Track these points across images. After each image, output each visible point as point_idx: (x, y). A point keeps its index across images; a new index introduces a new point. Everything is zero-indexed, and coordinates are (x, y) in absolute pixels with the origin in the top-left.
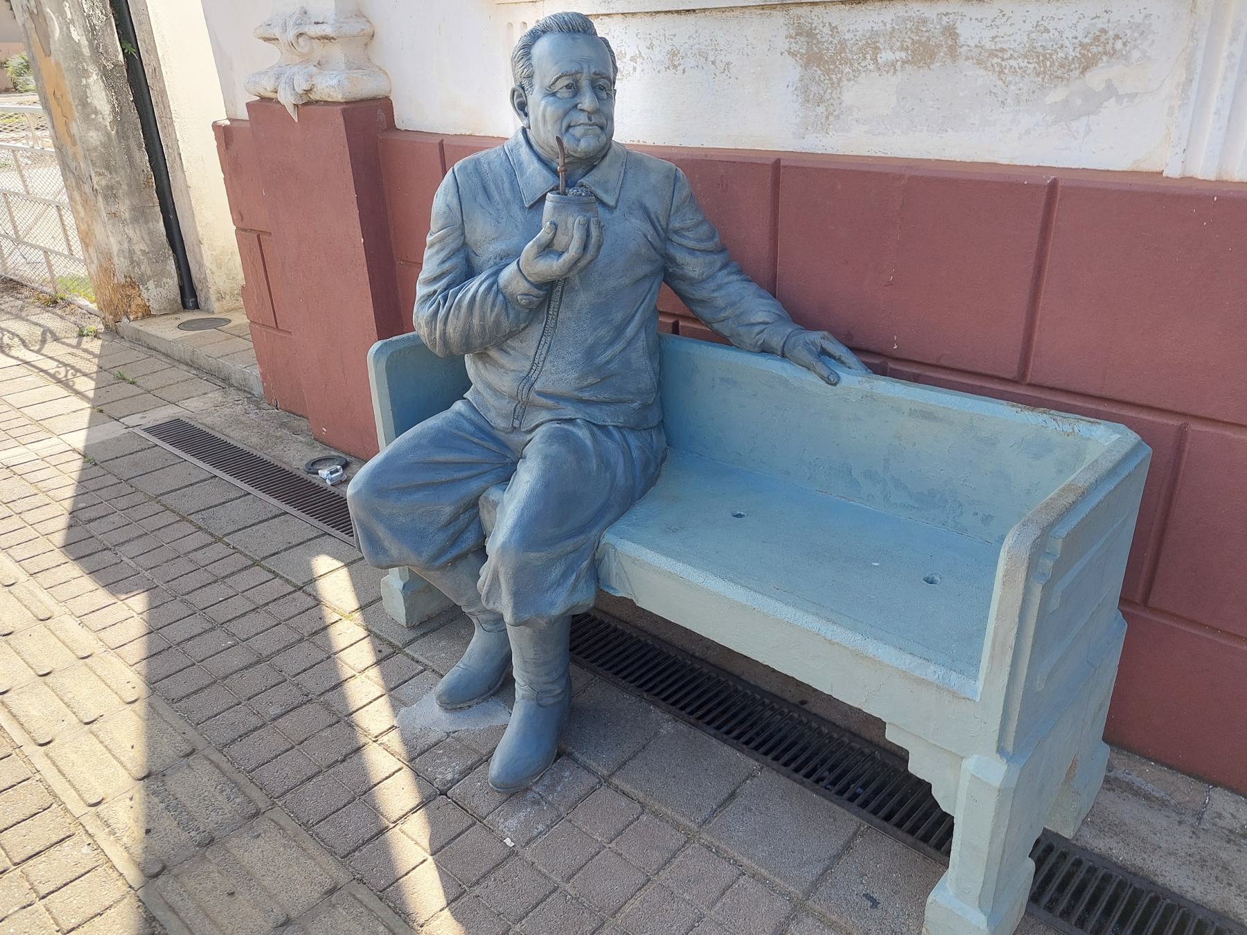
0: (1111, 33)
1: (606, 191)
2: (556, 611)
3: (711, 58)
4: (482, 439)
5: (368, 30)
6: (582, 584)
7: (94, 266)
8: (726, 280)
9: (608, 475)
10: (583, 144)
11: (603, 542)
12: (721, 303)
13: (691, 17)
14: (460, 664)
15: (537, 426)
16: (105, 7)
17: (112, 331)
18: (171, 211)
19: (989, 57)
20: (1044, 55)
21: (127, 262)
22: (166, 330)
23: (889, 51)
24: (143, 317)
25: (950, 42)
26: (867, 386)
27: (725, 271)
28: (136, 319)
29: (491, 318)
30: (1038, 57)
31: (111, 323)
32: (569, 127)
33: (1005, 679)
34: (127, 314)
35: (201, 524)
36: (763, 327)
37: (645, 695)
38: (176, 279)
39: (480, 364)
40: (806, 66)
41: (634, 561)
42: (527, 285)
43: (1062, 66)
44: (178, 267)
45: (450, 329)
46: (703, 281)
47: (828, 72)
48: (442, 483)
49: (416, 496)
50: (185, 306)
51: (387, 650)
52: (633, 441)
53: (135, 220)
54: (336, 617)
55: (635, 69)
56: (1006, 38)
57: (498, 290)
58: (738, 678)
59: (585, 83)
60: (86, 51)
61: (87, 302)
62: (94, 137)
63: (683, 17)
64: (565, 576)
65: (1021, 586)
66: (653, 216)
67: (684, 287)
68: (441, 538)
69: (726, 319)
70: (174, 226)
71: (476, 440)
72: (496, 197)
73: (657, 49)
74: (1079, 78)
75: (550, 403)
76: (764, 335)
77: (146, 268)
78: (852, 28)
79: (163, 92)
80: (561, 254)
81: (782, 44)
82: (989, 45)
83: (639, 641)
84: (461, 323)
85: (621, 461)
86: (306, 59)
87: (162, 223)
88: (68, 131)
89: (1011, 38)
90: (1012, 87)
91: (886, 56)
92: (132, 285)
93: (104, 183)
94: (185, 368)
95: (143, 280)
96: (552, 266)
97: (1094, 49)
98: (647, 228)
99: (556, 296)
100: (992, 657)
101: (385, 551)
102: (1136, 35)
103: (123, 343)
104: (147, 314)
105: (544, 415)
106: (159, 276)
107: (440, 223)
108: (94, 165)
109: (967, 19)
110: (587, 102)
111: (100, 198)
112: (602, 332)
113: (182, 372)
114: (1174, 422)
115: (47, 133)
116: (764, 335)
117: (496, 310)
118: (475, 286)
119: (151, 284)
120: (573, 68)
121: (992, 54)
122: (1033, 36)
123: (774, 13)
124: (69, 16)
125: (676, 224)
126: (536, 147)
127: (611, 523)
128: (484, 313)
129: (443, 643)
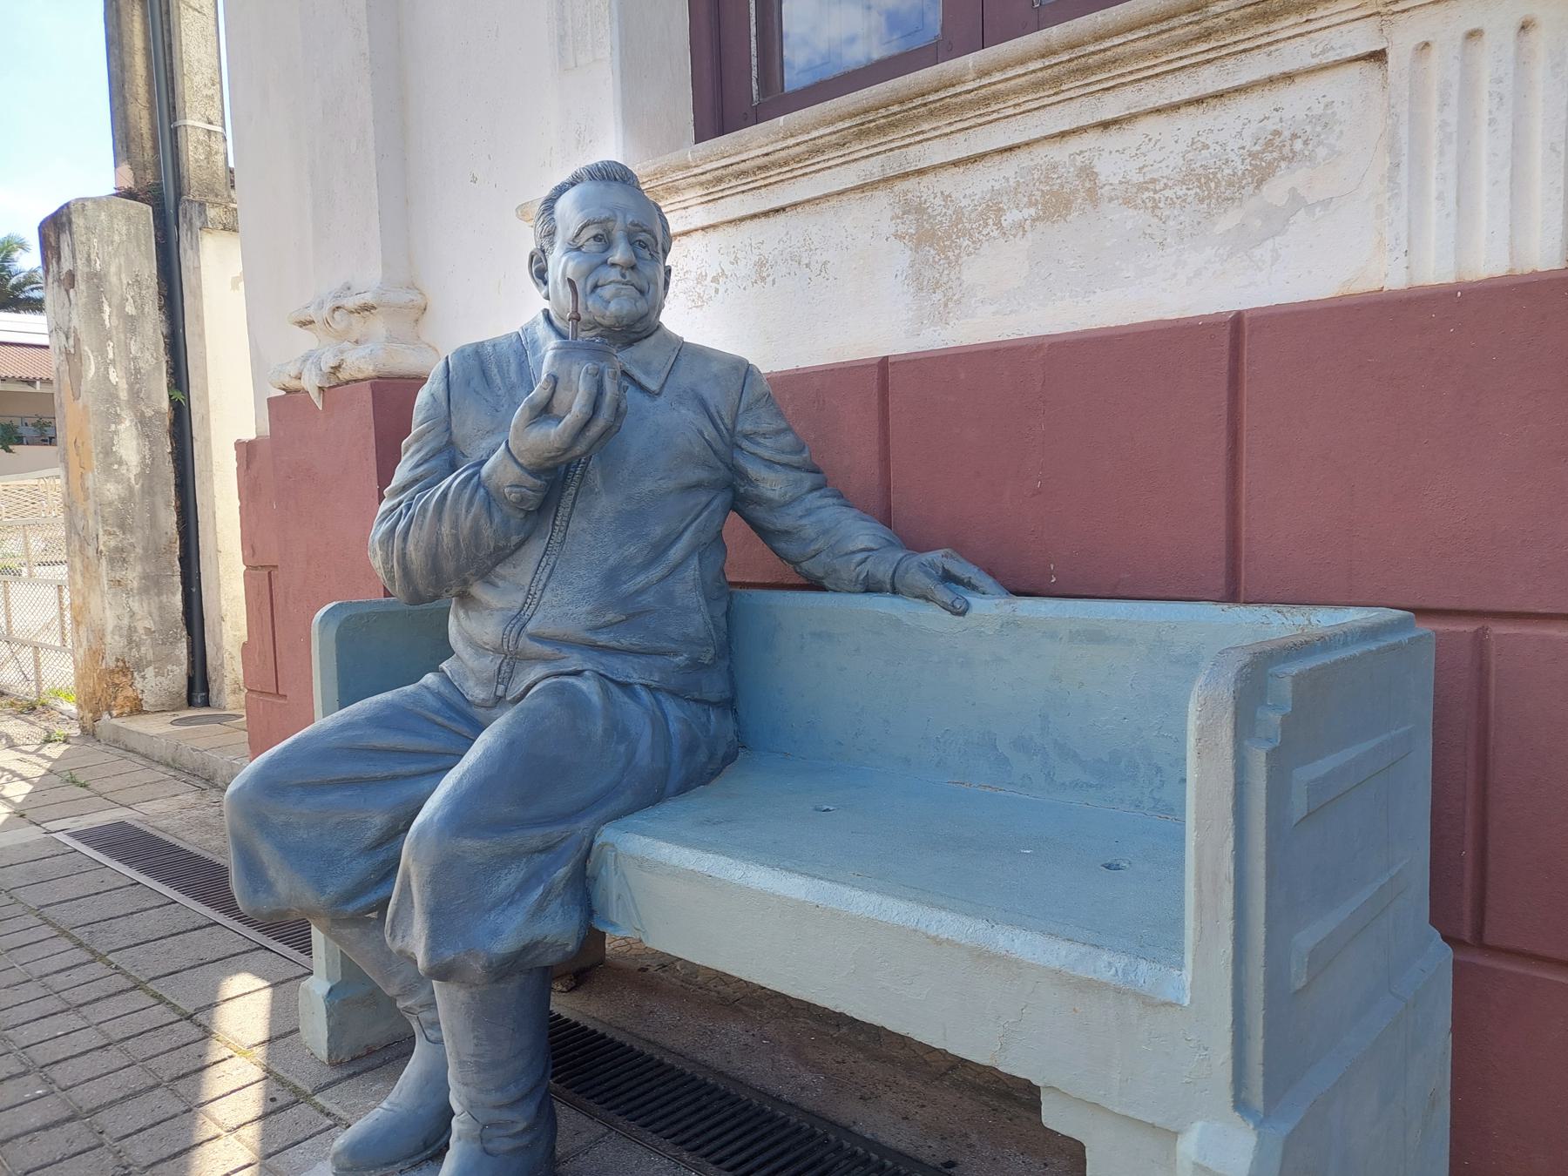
0: (1287, 134)
1: (647, 373)
2: (506, 944)
4: (449, 718)
5: (419, 301)
6: (555, 906)
7: (81, 651)
9: (622, 748)
10: (613, 307)
11: (598, 841)
12: (810, 532)
13: (781, 217)
14: (385, 1104)
15: (529, 688)
16: (157, 350)
17: (89, 733)
18: (195, 583)
20: (1207, 177)
21: (124, 642)
22: (156, 728)
23: (1015, 211)
24: (131, 713)
25: (1088, 185)
26: (1008, 608)
27: (817, 494)
28: (120, 715)
29: (466, 524)
30: (1199, 180)
31: (88, 725)
32: (596, 287)
33: (1227, 947)
34: (109, 709)
35: (85, 939)
36: (864, 555)
37: (685, 1155)
38: (185, 666)
39: (461, 613)
40: (916, 249)
41: (642, 863)
42: (517, 470)
43: (1230, 184)
44: (191, 653)
45: (411, 547)
47: (943, 250)
48: (375, 780)
50: (191, 703)
51: (284, 1098)
52: (671, 708)
53: (145, 590)
54: (226, 1052)
55: (717, 291)
56: (1157, 166)
57: (479, 484)
58: (847, 1130)
60: (124, 395)
61: (70, 707)
62: (112, 490)
63: (772, 220)
64: (524, 887)
65: (1229, 751)
66: (713, 410)
67: (760, 513)
69: (818, 553)
70: (195, 599)
71: (439, 720)
72: (498, 380)
73: (742, 263)
74: (1254, 194)
75: (547, 650)
77: (147, 651)
78: (968, 192)
79: (208, 442)
81: (887, 227)
82: (1137, 178)
83: (694, 1079)
84: (425, 533)
85: (648, 731)
86: (341, 336)
87: (179, 597)
88: (82, 485)
89: (1163, 165)
90: (1171, 223)
91: (1011, 217)
92: (125, 671)
93: (112, 544)
94: (163, 769)
95: (140, 665)
96: (552, 435)
97: (1268, 157)
98: (709, 432)
99: (567, 501)
100: (1200, 906)
101: (269, 887)
102: (1319, 129)
103: (98, 747)
104: (137, 709)
105: (538, 671)
106: (161, 662)
108: (105, 521)
109: (1105, 154)
110: (619, 254)
111: (104, 562)
113: (160, 772)
114: (1467, 627)
115: (58, 481)
116: (868, 566)
118: (452, 481)
119: (150, 672)
121: (1142, 188)
122: (1190, 156)
123: (876, 193)
124: (111, 356)
125: (746, 426)
126: (557, 323)
127: (617, 816)
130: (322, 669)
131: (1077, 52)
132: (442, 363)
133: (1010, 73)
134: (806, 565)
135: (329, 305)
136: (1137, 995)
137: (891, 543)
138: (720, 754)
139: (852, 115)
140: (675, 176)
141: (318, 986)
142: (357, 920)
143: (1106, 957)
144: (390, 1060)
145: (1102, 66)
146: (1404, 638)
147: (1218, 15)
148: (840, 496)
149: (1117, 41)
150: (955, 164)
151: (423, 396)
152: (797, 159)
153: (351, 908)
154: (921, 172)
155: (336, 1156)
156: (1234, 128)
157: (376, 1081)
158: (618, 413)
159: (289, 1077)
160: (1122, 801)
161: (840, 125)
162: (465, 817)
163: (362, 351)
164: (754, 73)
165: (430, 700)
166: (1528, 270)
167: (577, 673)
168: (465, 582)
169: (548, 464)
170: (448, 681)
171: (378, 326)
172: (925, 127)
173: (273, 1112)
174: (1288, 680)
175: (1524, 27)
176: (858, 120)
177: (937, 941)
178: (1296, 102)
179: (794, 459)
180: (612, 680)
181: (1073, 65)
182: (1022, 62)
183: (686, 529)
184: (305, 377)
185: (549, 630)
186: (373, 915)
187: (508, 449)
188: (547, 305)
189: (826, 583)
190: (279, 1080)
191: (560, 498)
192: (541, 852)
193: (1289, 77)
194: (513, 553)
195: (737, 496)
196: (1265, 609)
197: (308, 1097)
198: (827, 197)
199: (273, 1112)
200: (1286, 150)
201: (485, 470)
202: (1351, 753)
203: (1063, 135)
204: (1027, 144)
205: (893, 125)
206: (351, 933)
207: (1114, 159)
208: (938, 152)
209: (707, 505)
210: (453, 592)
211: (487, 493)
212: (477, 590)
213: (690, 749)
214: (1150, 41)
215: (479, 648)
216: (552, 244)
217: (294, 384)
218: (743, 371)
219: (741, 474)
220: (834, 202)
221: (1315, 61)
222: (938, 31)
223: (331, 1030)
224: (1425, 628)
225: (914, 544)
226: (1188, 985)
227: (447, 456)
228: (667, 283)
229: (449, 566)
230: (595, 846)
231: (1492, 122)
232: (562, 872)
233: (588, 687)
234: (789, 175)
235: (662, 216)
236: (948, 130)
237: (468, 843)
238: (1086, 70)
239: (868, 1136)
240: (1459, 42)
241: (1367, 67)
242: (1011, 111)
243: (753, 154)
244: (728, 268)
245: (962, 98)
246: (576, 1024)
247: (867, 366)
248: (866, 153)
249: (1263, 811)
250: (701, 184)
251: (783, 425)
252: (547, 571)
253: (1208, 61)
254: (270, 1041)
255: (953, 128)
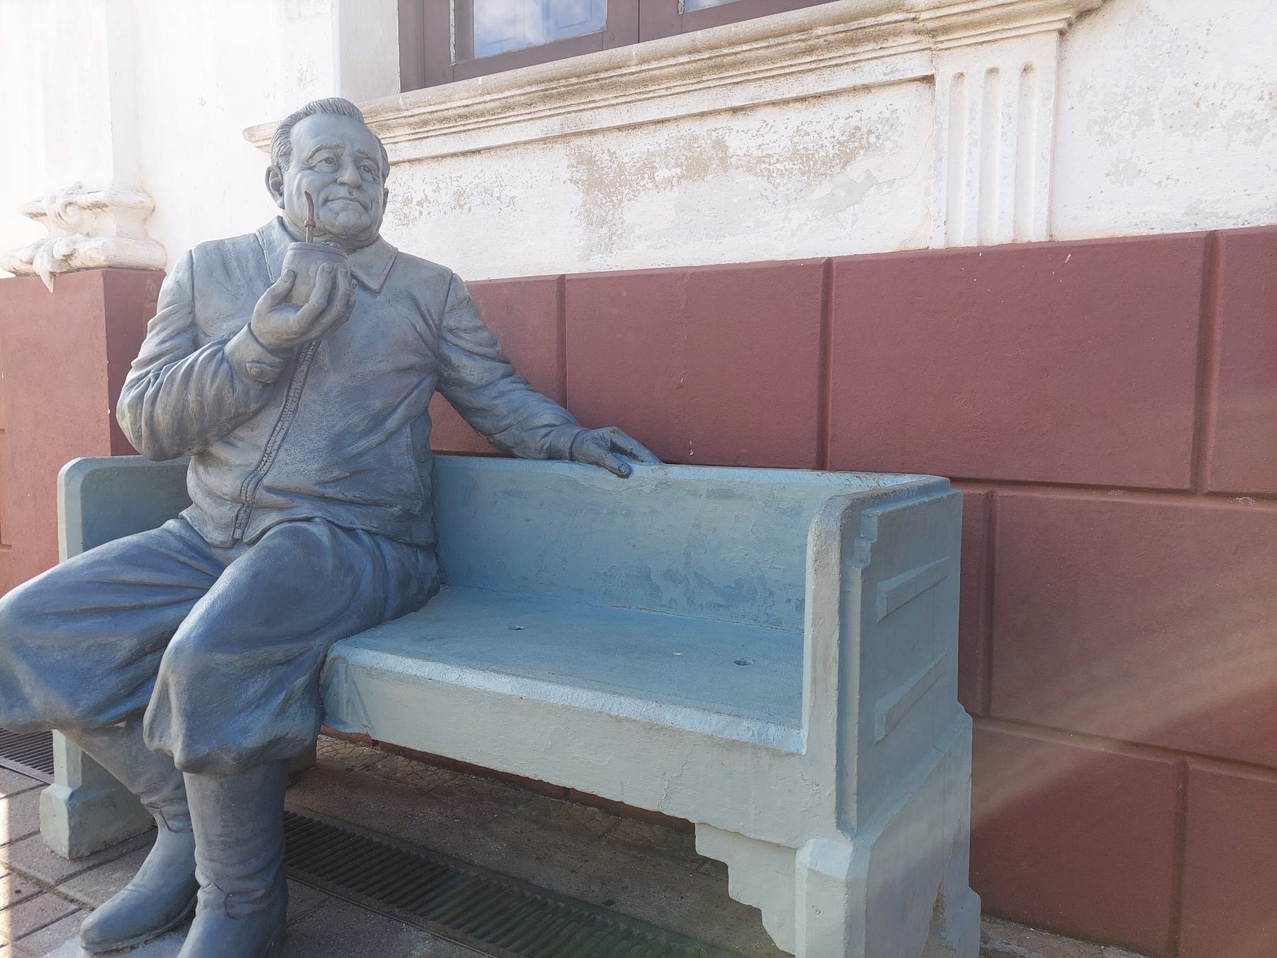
0: (864, 130)
1: (369, 275)
2: (253, 740)
3: (496, 194)
4: (191, 557)
8: (510, 387)
9: (349, 581)
10: (342, 218)
11: (331, 655)
12: (502, 410)
13: (477, 158)
14: (129, 887)
19: (759, 164)
20: (807, 156)
27: (508, 379)
29: (210, 392)
32: (326, 201)
33: (833, 695)
36: (549, 429)
37: (397, 911)
39: (201, 469)
40: (588, 192)
41: (370, 672)
42: (259, 349)
43: (824, 163)
45: (159, 410)
46: (485, 387)
48: (124, 609)
49: (83, 624)
51: (28, 889)
52: (388, 550)
55: (421, 213)
57: (223, 359)
59: (347, 160)
64: (269, 693)
65: (837, 569)
66: (424, 309)
67: (460, 393)
68: (111, 684)
71: (182, 558)
72: (237, 273)
75: (280, 500)
76: (550, 439)
80: (298, 308)
86: (73, 229)
90: (781, 188)
91: (662, 174)
96: (289, 321)
97: (851, 145)
98: (420, 325)
99: (299, 376)
100: (815, 682)
101: (23, 701)
105: (273, 517)
107: (166, 301)
109: (734, 132)
110: (348, 175)
112: (355, 419)
114: (981, 491)
116: (550, 439)
117: (218, 381)
120: (336, 142)
121: (760, 160)
122: (795, 140)
125: (450, 322)
126: (290, 228)
128: (203, 385)
129: (117, 875)
130: (67, 515)
131: (716, 52)
132: (185, 256)
133: (664, 63)
134: (498, 436)
135: (61, 201)
136: (768, 749)
137: (569, 421)
138: (426, 588)
139: (539, 82)
140: (387, 116)
141: (59, 790)
142: (107, 729)
143: (745, 724)
144: (127, 853)
145: (734, 65)
146: (945, 495)
147: (819, 37)
148: (526, 383)
149: (745, 47)
150: (619, 128)
151: (167, 284)
152: (492, 112)
153: (103, 719)
154: (592, 132)
155: (87, 932)
156: (827, 122)
157: (115, 871)
158: (349, 306)
159: (32, 872)
160: (744, 616)
161: (529, 89)
162: (217, 634)
163: (95, 243)
164: (452, 39)
165: (174, 543)
166: (1025, 240)
167: (308, 520)
168: (207, 442)
169: (287, 345)
170: (188, 526)
171: (109, 222)
172: (597, 97)
173: (19, 902)
174: (875, 519)
175: (1026, 70)
176: (543, 87)
177: (618, 720)
178: (873, 106)
179: (489, 351)
180: (338, 526)
181: (712, 62)
182: (673, 55)
183: (400, 403)
184: (37, 261)
185: (284, 482)
186: (122, 725)
187: (250, 331)
188: (281, 212)
189: (515, 451)
190: (21, 875)
191: (294, 374)
192: (282, 664)
193: (867, 88)
194: (251, 418)
195: (442, 380)
196: (848, 475)
197: (51, 888)
198: (516, 145)
199: (19, 902)
200: (864, 142)
201: (229, 347)
202: (912, 574)
203: (703, 114)
204: (675, 119)
205: (571, 94)
206: (100, 741)
207: (741, 137)
208: (606, 118)
209: (418, 385)
210: (195, 450)
211: (231, 367)
212: (217, 449)
213: (404, 583)
214: (769, 50)
215: (218, 498)
216: (288, 162)
217: (24, 268)
218: (448, 279)
219: (446, 361)
220: (521, 149)
221: (886, 79)
222: (604, 24)
223: (73, 830)
224: (960, 491)
225: (588, 422)
226: (805, 740)
227: (190, 335)
228: (385, 203)
229: (194, 428)
230: (328, 660)
231: (1003, 134)
232: (301, 681)
233: (320, 531)
234: (485, 124)
235: (381, 146)
236: (614, 102)
237: (221, 657)
238: (721, 67)
239: (545, 886)
240: (983, 75)
241: (922, 87)
242: (663, 92)
243: (455, 104)
244: (431, 195)
245: (627, 78)
246: (295, 815)
247: (548, 281)
248: (549, 113)
249: (859, 611)
250: (410, 125)
251: (480, 324)
252: (282, 433)
253: (811, 70)
254: (10, 843)
255: (619, 101)
